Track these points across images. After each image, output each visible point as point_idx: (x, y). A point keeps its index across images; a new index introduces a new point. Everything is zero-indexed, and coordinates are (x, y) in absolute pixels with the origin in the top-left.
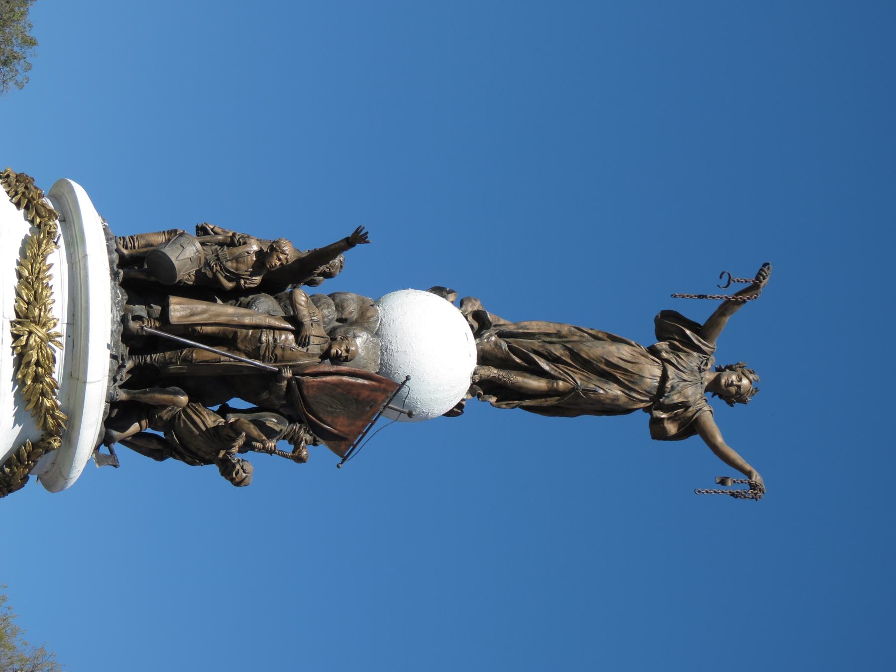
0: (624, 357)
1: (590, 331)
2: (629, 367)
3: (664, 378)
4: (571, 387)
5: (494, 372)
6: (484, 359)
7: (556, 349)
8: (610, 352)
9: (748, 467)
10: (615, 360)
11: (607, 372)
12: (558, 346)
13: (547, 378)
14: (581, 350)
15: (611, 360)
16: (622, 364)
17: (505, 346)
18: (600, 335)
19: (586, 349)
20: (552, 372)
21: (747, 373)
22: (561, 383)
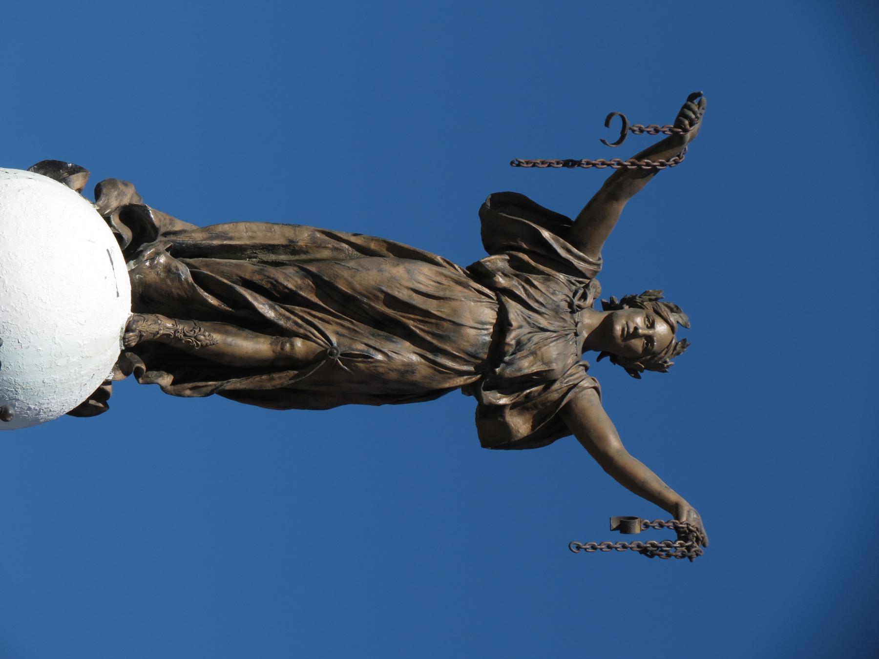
0: (422, 288)
1: (353, 239)
2: (431, 306)
3: (502, 325)
4: (320, 349)
5: (166, 325)
6: (145, 300)
7: (287, 277)
8: (393, 279)
9: (672, 496)
10: (403, 295)
11: (389, 317)
12: (291, 270)
13: (271, 334)
14: (337, 276)
15: (396, 293)
16: (418, 301)
17: (185, 273)
18: (373, 246)
19: (346, 274)
20: (282, 322)
21: (665, 311)
22: (299, 343)
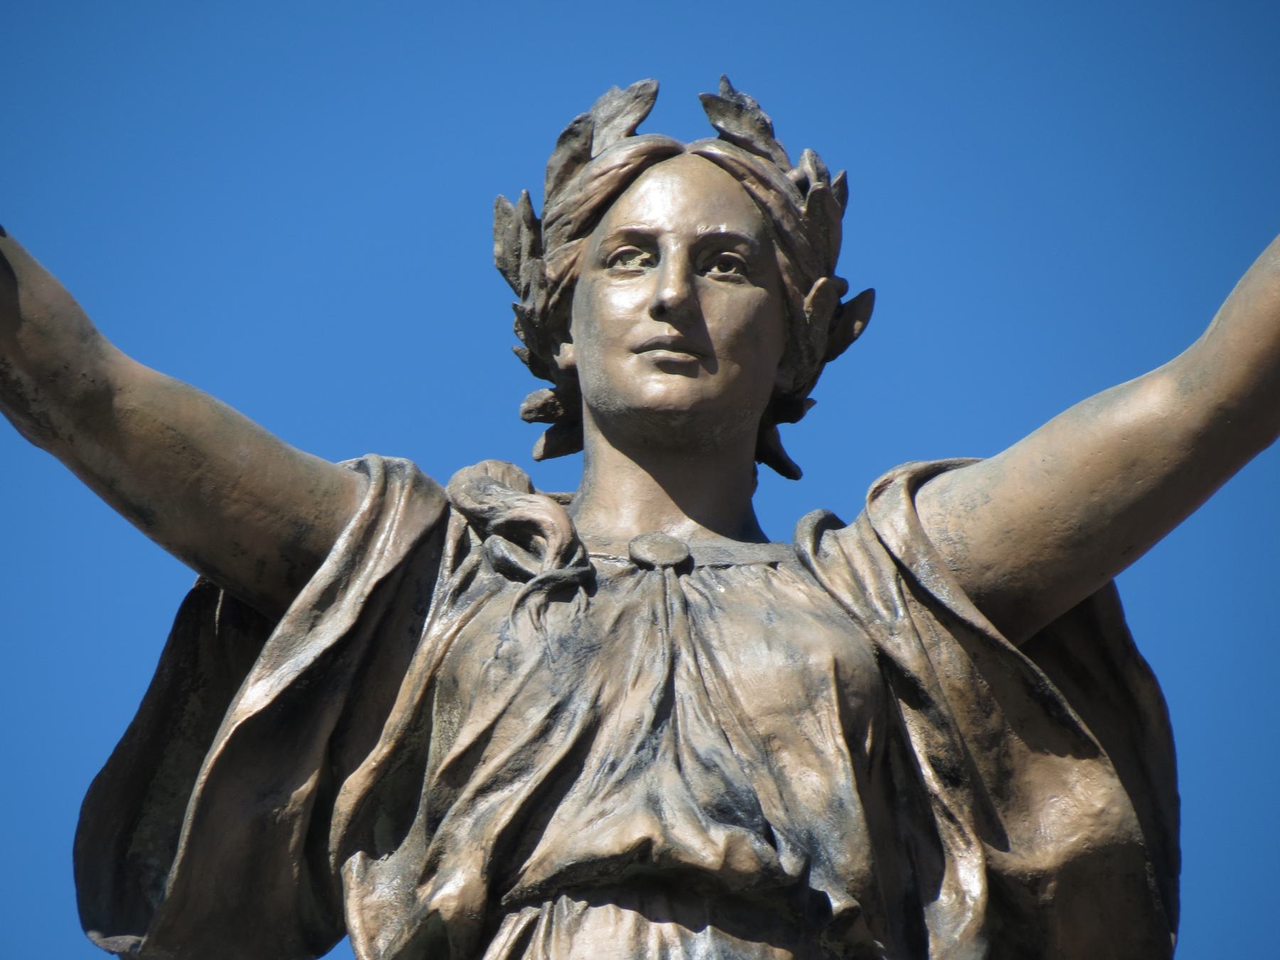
21: (585, 187)
